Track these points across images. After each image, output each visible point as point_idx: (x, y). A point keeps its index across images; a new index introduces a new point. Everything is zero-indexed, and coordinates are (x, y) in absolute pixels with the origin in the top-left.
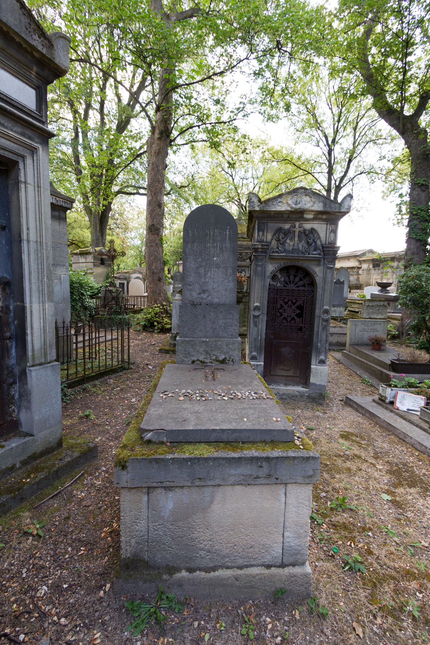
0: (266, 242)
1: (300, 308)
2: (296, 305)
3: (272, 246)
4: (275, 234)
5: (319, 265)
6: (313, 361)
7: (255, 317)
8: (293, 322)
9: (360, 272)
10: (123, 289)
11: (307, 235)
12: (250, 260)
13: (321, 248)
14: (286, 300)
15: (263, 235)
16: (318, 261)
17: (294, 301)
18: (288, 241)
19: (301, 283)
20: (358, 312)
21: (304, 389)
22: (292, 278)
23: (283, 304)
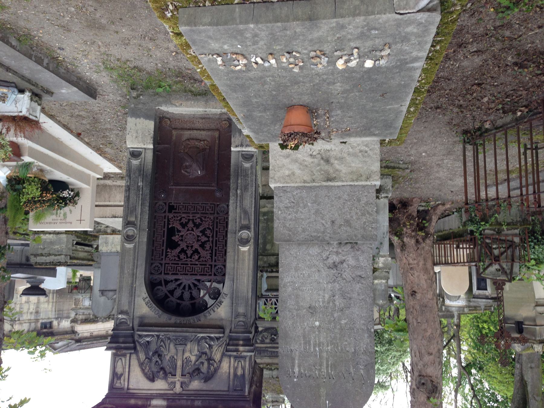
0: (230, 356)
1: (172, 245)
2: (178, 250)
3: (221, 349)
4: (216, 370)
5: (142, 318)
6: (149, 156)
7: (248, 228)
8: (184, 221)
9: (73, 315)
10: (478, 274)
11: (162, 369)
12: (257, 328)
13: (138, 348)
14: (197, 257)
15: (236, 369)
16: (144, 324)
17: (198, 221)
18: (193, 359)
19: (171, 286)
20: (78, 244)
21: (164, 108)
22: (187, 295)
23: (200, 250)
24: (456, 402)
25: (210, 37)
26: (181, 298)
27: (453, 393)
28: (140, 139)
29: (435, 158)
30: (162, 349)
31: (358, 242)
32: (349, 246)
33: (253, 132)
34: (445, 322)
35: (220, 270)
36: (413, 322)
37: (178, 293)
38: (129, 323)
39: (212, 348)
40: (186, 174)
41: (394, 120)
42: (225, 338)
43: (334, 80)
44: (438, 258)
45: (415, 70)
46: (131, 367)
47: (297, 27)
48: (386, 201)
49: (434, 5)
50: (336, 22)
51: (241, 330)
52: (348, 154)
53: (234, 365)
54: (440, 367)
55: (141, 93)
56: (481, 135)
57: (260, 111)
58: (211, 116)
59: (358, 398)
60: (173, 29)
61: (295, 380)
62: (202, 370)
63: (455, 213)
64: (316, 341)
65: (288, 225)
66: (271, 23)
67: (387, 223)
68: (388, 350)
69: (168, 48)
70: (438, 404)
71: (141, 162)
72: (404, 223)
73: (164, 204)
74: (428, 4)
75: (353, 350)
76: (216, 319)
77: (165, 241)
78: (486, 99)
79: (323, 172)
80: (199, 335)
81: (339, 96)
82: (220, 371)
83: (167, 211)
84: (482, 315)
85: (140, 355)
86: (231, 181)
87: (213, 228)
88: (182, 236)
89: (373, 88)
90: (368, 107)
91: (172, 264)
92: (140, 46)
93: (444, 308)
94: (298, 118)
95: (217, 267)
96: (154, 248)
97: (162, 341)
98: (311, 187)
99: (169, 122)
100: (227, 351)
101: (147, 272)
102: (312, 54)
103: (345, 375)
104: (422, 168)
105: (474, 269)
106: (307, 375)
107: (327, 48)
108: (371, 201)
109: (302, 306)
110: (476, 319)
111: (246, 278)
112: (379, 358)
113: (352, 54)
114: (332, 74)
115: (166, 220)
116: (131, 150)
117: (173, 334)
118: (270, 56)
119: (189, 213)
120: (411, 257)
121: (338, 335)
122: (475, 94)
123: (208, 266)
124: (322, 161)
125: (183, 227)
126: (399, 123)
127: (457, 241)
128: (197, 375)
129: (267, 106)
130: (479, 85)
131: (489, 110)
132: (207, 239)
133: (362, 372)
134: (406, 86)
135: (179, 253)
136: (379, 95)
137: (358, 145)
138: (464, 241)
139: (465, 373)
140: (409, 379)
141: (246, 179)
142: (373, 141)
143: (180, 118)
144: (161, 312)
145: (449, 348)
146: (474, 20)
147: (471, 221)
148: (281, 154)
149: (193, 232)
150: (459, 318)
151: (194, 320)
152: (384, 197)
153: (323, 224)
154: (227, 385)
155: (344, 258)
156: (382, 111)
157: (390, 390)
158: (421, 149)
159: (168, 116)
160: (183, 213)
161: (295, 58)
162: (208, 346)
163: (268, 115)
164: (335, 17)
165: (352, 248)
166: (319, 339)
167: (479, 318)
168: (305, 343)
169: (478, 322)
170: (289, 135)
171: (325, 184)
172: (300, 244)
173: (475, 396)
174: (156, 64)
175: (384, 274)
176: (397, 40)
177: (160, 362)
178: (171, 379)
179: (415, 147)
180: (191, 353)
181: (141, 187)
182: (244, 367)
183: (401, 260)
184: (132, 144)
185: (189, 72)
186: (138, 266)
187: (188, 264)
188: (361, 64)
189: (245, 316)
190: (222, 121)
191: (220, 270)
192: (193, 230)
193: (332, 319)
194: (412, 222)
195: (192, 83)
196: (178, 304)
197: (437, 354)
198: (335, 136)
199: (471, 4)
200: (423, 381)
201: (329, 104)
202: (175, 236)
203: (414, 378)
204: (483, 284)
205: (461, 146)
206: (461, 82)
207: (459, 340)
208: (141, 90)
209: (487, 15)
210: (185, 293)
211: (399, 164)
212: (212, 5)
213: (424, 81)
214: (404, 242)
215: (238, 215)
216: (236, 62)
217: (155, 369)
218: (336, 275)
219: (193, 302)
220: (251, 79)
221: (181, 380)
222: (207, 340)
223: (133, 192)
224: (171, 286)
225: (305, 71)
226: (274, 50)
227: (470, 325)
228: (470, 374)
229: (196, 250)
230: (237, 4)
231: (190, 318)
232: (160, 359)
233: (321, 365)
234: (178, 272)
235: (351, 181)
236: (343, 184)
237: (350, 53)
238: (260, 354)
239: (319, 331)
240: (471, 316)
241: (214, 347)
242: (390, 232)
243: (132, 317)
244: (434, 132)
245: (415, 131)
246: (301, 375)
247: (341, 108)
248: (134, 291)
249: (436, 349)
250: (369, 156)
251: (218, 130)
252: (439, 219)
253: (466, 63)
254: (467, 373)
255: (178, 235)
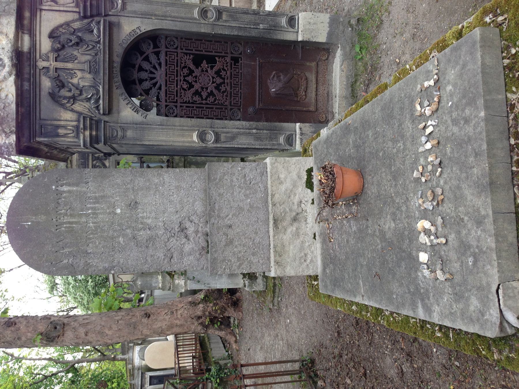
0: (78, 121)
2: (192, 67)
3: (86, 111)
4: (63, 106)
5: (119, 25)
6: (290, 37)
7: (217, 140)
8: (223, 73)
11: (63, 47)
13: (86, 21)
14: (185, 86)
15: (65, 127)
16: (111, 28)
18: (75, 81)
19: (153, 59)
21: (339, 53)
23: (193, 90)
24: (39, 359)
25: (464, 66)
26: (141, 69)
27: (48, 357)
28: (308, 27)
29: (284, 332)
30: (85, 47)
31: (209, 255)
32: (204, 244)
33: (328, 137)
34: (118, 346)
35: (171, 111)
36: (119, 316)
37: (146, 65)
38: (113, 11)
39: (87, 101)
40: (272, 76)
41: (344, 288)
42: (98, 116)
43: (399, 219)
44: (182, 338)
45: (413, 309)
46: (64, 13)
47: (480, 169)
48: (241, 286)
49: (506, 328)
50: (488, 215)
51: (108, 132)
52: (302, 242)
53: (69, 125)
54: (73, 344)
55: (354, 29)
56: (310, 377)
57: (354, 142)
58: (330, 103)
59: (35, 257)
60: (467, 27)
61: (54, 187)
62: (62, 90)
63: (227, 353)
64: (98, 210)
65: (226, 177)
66: (486, 137)
67: (219, 287)
68: (89, 292)
69: (403, 53)
70: (36, 344)
71: (284, 27)
72: (218, 304)
73: (240, 52)
74: (507, 322)
75: (89, 251)
76: (119, 106)
77: (201, 53)
78: (348, 381)
79: (283, 215)
80: (101, 87)
81: (376, 227)
82: (62, 110)
83: (233, 55)
84: (125, 381)
85: (78, 23)
86: (265, 123)
87: (216, 104)
88: (207, 71)
89: (388, 263)
90: (361, 260)
91: (177, 60)
92: (406, 24)
93: (131, 345)
94: (349, 182)
95: (174, 108)
96: (193, 40)
97: (94, 47)
98: (267, 202)
99: (324, 58)
100: (84, 117)
101: (167, 33)
102: (439, 191)
103: (61, 243)
104: (273, 320)
105: (173, 372)
106: (60, 201)
107: (447, 208)
108: (254, 267)
109: (138, 194)
110: (121, 376)
111: (164, 138)
112: (81, 284)
113: (437, 237)
114: (408, 217)
115: (223, 54)
116: (297, 17)
117: (102, 59)
118: (435, 142)
119: (231, 79)
120: (183, 311)
121: (106, 234)
122: (354, 370)
123: (176, 98)
124: (294, 214)
125: (216, 73)
126: (339, 295)
127: (200, 356)
128: (57, 85)
129: (362, 148)
130: (365, 374)
131: (337, 385)
132: (204, 98)
133: (65, 261)
134: (390, 300)
135: (189, 68)
136: (378, 271)
137: (312, 252)
138: (200, 363)
139: (69, 367)
140: (61, 314)
141: (267, 138)
142: (316, 267)
143: (328, 70)
144: (125, 46)
145: (92, 351)
146: (438, 368)
147: (220, 369)
148: (302, 170)
149: (211, 83)
150: (122, 360)
151: (117, 82)
152: (245, 283)
153: (227, 216)
154: (45, 118)
155: (191, 239)
156: (355, 276)
157: (49, 295)
158: (293, 318)
159: (330, 57)
160: (231, 73)
161: (433, 172)
162: (89, 96)
163: (350, 150)
164: (494, 212)
165: (203, 247)
166: (101, 213)
167: (122, 379)
168: (96, 198)
169: (118, 377)
170: (332, 173)
171: (271, 217)
172: (206, 192)
173: (46, 377)
174: (386, 43)
175: (168, 286)
176: (458, 288)
177: (70, 44)
178: (52, 56)
179: (295, 312)
180: (81, 78)
181: (258, 27)
182: (67, 138)
183: (180, 302)
184: (303, 18)
185: (377, 78)
186: (174, 22)
187: (177, 77)
188: (423, 248)
189: (123, 138)
190: (325, 114)
191: (171, 111)
192: (213, 82)
193: (124, 227)
194: (219, 311)
195: (364, 82)
196: (134, 66)
197: (86, 341)
198: (323, 227)
199: (458, 365)
200: (58, 327)
201: (365, 216)
202: (207, 63)
203: (61, 319)
204: (155, 381)
205: (297, 358)
206: (368, 357)
207: (100, 361)
208: (357, 29)
209: (444, 382)
210: (146, 73)
211: (278, 297)
212: (504, 68)
213: (392, 319)
214: (198, 304)
215: (230, 130)
216: (426, 103)
217: (62, 39)
218: (173, 231)
219: (137, 82)
220: (400, 125)
221: (52, 68)
222: (96, 96)
223: (253, 18)
224: (153, 59)
225: (413, 185)
226: (445, 146)
227: (115, 371)
228: (68, 372)
229: (193, 86)
230: (506, 97)
231: (120, 78)
232: (74, 44)
233: (71, 215)
234: (168, 66)
235: (274, 245)
236: (271, 237)
237: (438, 235)
238: (82, 164)
239: (110, 213)
240: (124, 371)
241: (88, 103)
242: (208, 290)
243: (119, 14)
244: (312, 330)
245: (313, 311)
246: (60, 193)
247: (360, 231)
248: (147, 17)
249: (91, 340)
250: (301, 264)
251: (317, 110)
252: (221, 338)
253: (389, 361)
254: (69, 369)
255: (208, 67)
